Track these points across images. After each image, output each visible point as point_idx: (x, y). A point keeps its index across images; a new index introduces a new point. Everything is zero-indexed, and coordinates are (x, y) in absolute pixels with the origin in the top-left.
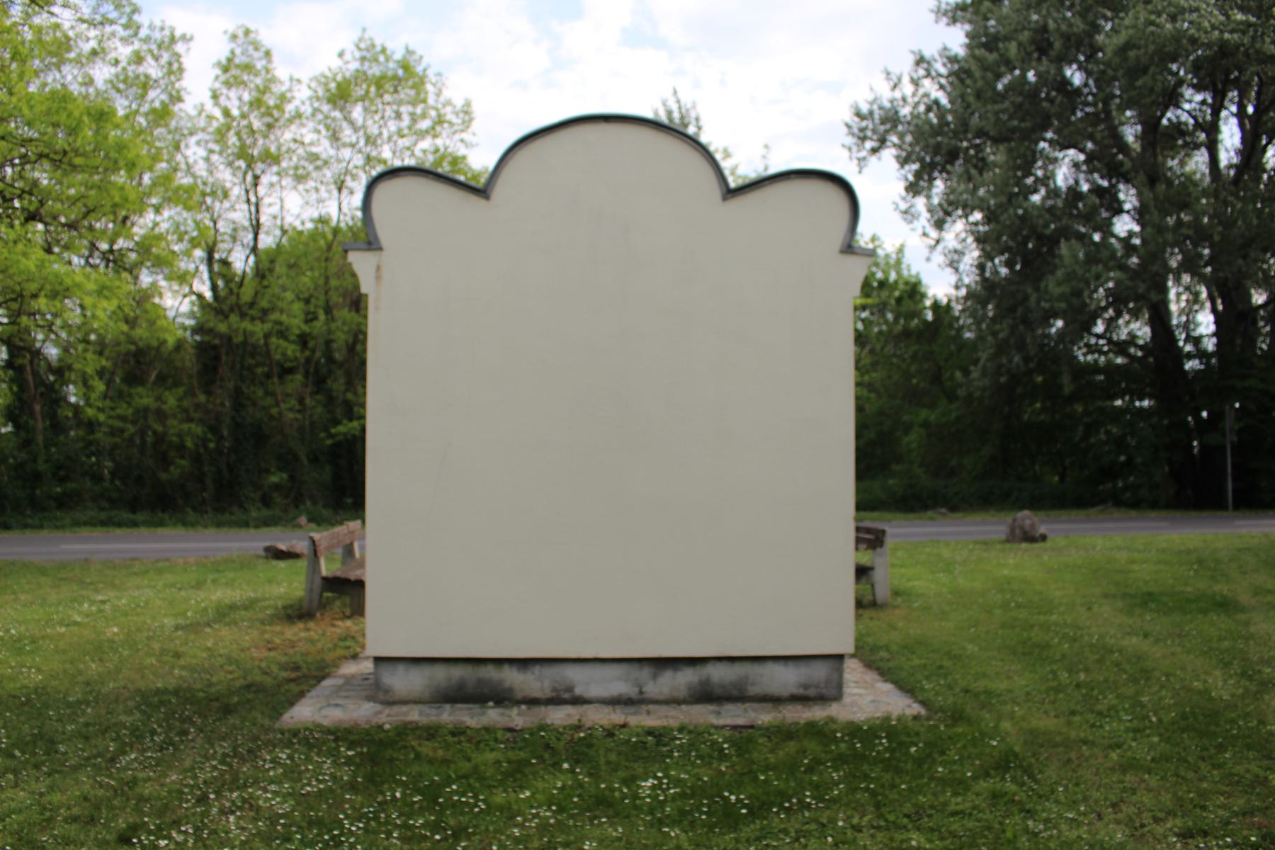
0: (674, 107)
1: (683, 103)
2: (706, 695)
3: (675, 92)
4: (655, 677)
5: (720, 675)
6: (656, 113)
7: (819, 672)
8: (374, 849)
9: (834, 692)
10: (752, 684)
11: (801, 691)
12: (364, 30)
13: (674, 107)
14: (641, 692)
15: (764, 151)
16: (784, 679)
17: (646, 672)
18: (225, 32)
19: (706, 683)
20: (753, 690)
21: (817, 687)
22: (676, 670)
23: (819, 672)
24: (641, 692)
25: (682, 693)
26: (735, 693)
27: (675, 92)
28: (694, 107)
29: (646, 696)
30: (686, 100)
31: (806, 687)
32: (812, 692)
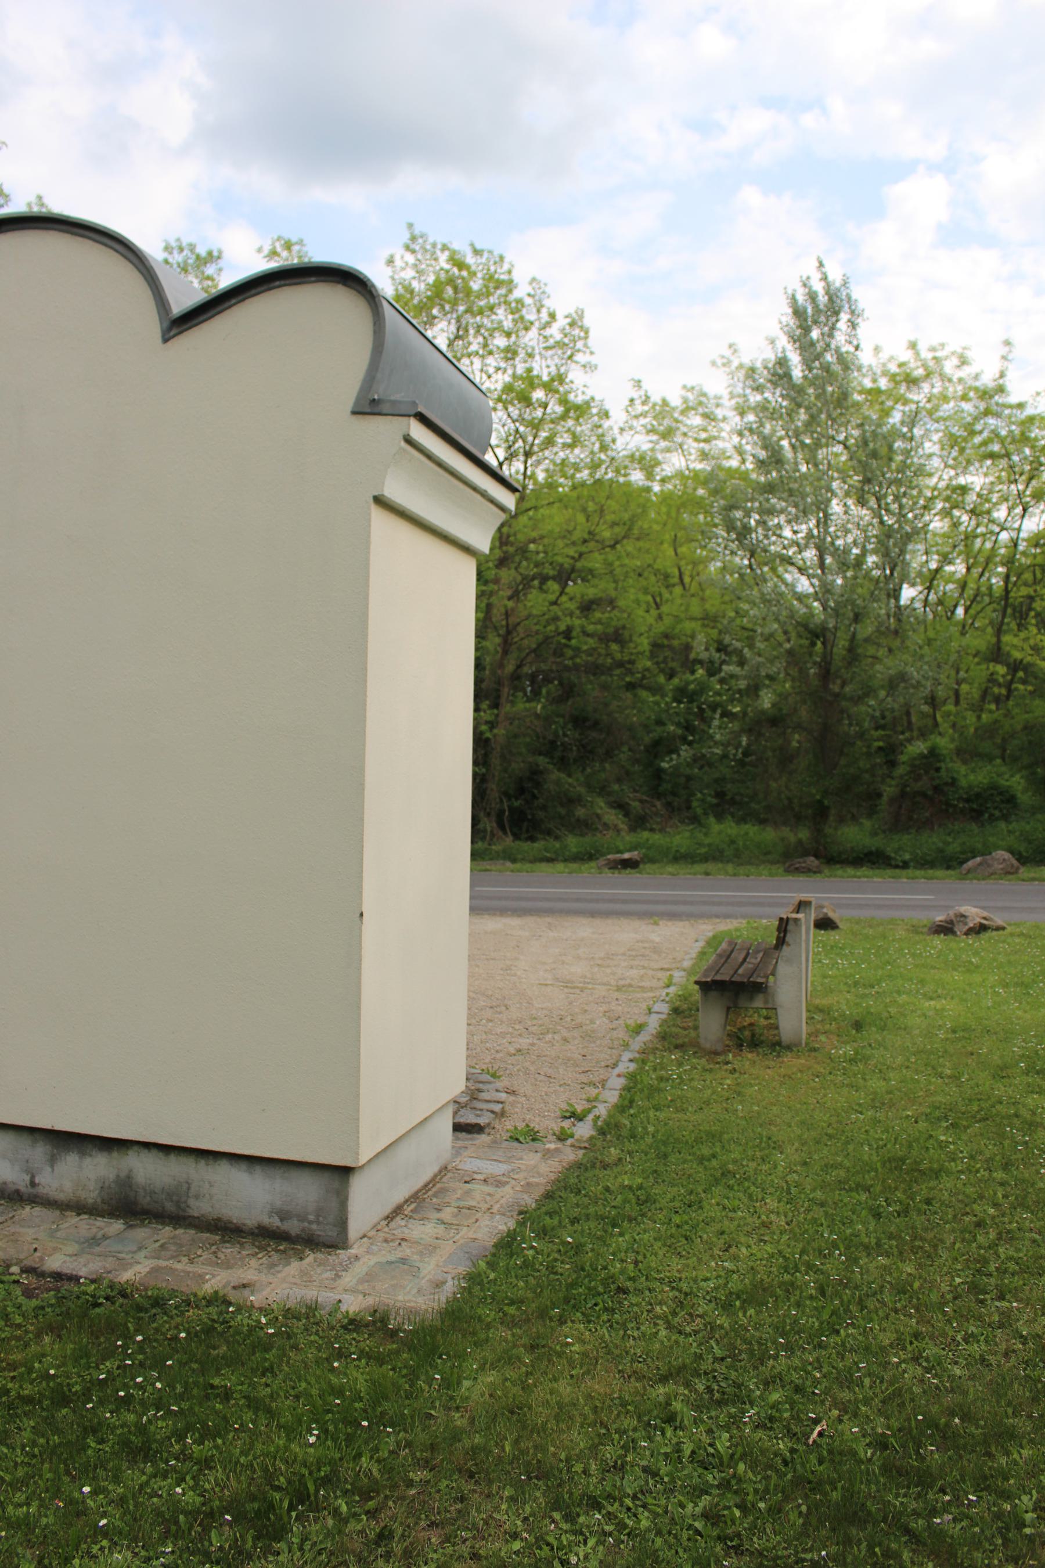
0: (818, 287)
1: (830, 278)
2: (127, 1206)
3: (821, 265)
4: (53, 1160)
5: (147, 1171)
6: (29, 205)
7: (306, 1192)
8: (1044, 1505)
9: (329, 1233)
10: (197, 1197)
11: (276, 1222)
12: (410, 226)
13: (818, 287)
14: (33, 1184)
15: (1004, 350)
16: (248, 1197)
17: (39, 1151)
18: (260, 250)
19: (126, 1182)
20: (199, 1208)
21: (302, 1218)
22: (83, 1154)
23: (306, 1192)
24: (33, 1184)
25: (91, 1195)
26: (170, 1207)
27: (821, 265)
28: (845, 283)
29: (40, 1190)
30: (835, 277)
31: (284, 1215)
32: (293, 1227)
